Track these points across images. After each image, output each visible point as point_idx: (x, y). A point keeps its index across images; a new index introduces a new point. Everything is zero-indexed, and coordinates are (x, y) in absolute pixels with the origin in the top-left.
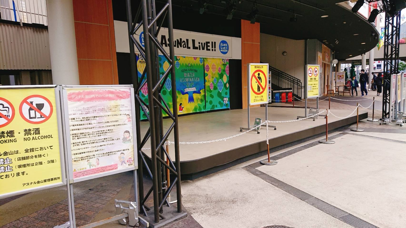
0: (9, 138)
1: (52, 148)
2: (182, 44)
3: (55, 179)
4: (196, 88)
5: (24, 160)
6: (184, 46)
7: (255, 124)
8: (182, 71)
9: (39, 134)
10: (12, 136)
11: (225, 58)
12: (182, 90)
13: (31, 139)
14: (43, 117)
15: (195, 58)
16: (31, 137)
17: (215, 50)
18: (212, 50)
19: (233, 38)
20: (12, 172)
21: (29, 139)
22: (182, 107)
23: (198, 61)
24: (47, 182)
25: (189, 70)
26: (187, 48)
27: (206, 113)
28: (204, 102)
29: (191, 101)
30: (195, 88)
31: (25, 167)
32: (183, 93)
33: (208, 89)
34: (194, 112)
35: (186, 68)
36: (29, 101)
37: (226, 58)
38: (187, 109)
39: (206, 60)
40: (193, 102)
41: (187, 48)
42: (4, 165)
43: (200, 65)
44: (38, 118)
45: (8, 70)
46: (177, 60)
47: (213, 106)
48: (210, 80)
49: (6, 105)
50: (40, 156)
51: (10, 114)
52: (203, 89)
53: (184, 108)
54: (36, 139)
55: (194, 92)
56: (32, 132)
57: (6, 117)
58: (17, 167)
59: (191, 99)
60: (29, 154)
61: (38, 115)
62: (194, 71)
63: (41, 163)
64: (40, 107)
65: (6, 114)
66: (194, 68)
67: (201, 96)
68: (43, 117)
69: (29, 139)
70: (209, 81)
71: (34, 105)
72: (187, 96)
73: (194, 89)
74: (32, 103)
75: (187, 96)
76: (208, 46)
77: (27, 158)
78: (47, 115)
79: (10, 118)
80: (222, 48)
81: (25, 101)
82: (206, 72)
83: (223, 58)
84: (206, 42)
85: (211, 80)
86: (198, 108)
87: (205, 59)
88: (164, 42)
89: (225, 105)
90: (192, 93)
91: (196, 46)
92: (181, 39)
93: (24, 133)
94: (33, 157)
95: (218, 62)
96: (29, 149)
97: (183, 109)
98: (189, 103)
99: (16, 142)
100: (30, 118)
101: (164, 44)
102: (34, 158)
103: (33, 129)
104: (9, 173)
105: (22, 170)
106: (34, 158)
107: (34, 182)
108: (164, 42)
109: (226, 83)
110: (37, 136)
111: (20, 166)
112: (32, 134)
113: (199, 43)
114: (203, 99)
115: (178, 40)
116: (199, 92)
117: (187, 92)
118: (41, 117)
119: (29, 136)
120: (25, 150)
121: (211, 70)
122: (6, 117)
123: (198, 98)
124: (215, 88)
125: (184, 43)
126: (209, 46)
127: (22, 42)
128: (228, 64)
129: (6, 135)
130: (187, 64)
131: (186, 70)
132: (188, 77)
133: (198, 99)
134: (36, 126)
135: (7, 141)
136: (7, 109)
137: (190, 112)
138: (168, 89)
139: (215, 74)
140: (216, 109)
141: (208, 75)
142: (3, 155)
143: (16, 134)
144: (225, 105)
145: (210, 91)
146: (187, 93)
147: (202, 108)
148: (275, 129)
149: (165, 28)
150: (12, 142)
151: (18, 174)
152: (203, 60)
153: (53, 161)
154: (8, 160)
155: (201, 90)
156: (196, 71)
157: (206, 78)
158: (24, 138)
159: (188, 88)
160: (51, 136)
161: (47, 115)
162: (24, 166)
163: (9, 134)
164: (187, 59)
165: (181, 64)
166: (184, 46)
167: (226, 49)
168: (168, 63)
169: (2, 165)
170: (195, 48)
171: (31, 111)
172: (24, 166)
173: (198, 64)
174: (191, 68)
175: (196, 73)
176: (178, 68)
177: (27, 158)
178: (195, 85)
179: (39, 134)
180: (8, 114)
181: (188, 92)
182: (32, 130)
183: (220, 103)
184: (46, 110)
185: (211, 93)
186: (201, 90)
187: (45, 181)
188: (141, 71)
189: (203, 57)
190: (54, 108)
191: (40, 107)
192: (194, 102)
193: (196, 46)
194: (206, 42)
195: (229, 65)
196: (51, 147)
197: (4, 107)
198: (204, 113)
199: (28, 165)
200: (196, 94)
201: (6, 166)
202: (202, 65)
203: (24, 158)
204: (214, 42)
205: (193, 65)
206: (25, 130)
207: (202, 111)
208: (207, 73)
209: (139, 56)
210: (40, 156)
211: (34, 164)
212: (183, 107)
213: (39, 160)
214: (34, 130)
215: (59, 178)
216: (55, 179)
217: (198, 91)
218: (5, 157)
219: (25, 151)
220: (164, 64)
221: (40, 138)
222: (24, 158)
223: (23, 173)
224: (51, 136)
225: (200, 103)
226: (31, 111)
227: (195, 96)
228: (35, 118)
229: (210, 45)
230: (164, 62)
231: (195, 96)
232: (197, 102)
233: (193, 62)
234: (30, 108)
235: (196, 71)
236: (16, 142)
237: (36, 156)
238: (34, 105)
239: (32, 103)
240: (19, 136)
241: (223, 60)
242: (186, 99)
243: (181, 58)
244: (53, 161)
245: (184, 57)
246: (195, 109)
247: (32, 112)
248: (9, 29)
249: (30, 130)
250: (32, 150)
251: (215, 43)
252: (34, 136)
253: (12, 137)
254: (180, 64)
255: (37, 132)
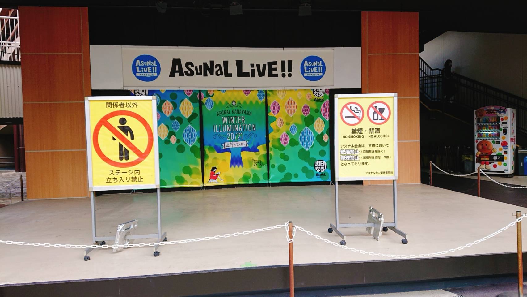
0: (359, 134)
1: (388, 145)
2: (215, 70)
3: (389, 172)
4: (247, 142)
5: (368, 153)
6: (219, 73)
7: (368, 222)
8: (218, 114)
9: (380, 133)
10: (361, 133)
11: (318, 88)
12: (218, 145)
13: (374, 136)
14: (383, 119)
15: (247, 92)
16: (374, 134)
17: (290, 75)
18: (284, 76)
19: (337, 49)
20: (359, 161)
21: (372, 136)
22: (216, 173)
23: (254, 96)
24: (383, 174)
25: (233, 111)
26: (225, 76)
27: (270, 187)
28: (265, 169)
29: (236, 164)
30: (245, 141)
31: (368, 158)
32: (220, 151)
33: (277, 144)
34: (243, 183)
35: (226, 109)
36: (374, 106)
37: (322, 88)
38: (227, 178)
39: (273, 94)
40: (240, 166)
41: (225, 76)
42: (355, 155)
43: (257, 102)
44: (380, 120)
45: (17, 118)
46: (208, 95)
47: (289, 175)
48: (281, 128)
49: (359, 108)
50: (379, 151)
51: (361, 116)
52: (264, 144)
53: (219, 175)
54: (377, 137)
55: (244, 149)
56: (375, 131)
57: (358, 118)
58: (363, 158)
59: (236, 161)
60: (372, 149)
61: (380, 118)
62: (245, 113)
63: (379, 157)
64: (382, 110)
65: (359, 116)
66: (246, 109)
67: (258, 156)
68: (383, 119)
69: (372, 136)
70: (278, 130)
71: (378, 109)
72: (228, 156)
73: (244, 144)
74: (376, 107)
75: (228, 156)
76: (271, 70)
77: (370, 151)
78: (386, 118)
79: (360, 118)
80: (308, 70)
81: (371, 106)
82: (271, 114)
83: (315, 88)
84: (268, 62)
85: (284, 129)
86: (252, 176)
87: (268, 92)
88: (177, 69)
89: (317, 174)
90: (240, 150)
91: (244, 70)
92: (212, 62)
93: (352, 132)
94: (374, 151)
95: (303, 95)
96: (371, 144)
97: (218, 177)
98: (231, 166)
99: (363, 137)
100: (374, 119)
101: (177, 72)
102: (375, 152)
103: (376, 129)
104: (357, 162)
105: (365, 161)
106: (375, 152)
107: (374, 172)
108: (177, 69)
109: (322, 134)
110: (378, 134)
111: (364, 158)
112: (374, 133)
113: (252, 65)
114: (264, 161)
115: (205, 64)
116: (255, 150)
117: (229, 149)
118: (382, 120)
119: (372, 134)
120: (369, 145)
121: (283, 110)
122: (358, 118)
123: (253, 160)
124: (293, 143)
125: (218, 68)
126: (275, 69)
127: (9, 85)
128: (329, 98)
129: (357, 131)
130: (230, 103)
131: (226, 112)
132: (230, 124)
133: (251, 161)
134: (378, 127)
135: (358, 136)
136: (359, 112)
137: (234, 182)
138: (188, 144)
139: (293, 117)
140: (293, 180)
141: (277, 120)
142: (354, 147)
143: (364, 131)
144: (317, 174)
145: (282, 148)
146: (228, 150)
147: (261, 177)
148: (404, 242)
149: (179, 47)
150: (361, 137)
151: (363, 164)
152: (266, 94)
153: (388, 157)
154: (357, 151)
155: (259, 145)
156: (248, 113)
157: (272, 125)
158: (369, 136)
159: (229, 143)
160: (388, 136)
161: (386, 118)
162: (368, 157)
163: (359, 131)
164: (229, 94)
165: (217, 103)
166: (219, 73)
167: (318, 71)
168: (190, 102)
169: (353, 155)
170: (241, 73)
171: (375, 114)
172: (368, 157)
173: (254, 102)
174: (238, 108)
175: (247, 116)
176: (210, 110)
177: (370, 151)
178: (247, 137)
179: (380, 133)
180: (360, 116)
181: (231, 150)
182: (374, 129)
183: (304, 170)
184: (385, 114)
185: (282, 152)
186: (259, 146)
187: (381, 173)
188: (185, 114)
189: (265, 89)
190: (392, 112)
191: (382, 110)
192: (242, 166)
193: (244, 70)
194: (268, 62)
195: (330, 100)
196: (387, 144)
197: (357, 110)
198: (266, 186)
199: (370, 157)
200: (247, 152)
201: (356, 155)
202: (262, 103)
203: (368, 152)
204: (288, 61)
205: (242, 103)
206: (370, 129)
207: (260, 182)
208: (275, 116)
209: (316, 167)
210: (379, 151)
211: (375, 158)
212: (217, 174)
213: (378, 154)
214: (376, 129)
215: (392, 172)
216: (389, 172)
217: (253, 147)
218: (356, 149)
219: (368, 146)
220: (182, 104)
221: (380, 136)
222: (368, 152)
223: (366, 163)
224: (388, 136)
225: (256, 168)
226: (375, 114)
227: (245, 156)
228: (377, 119)
229: (279, 66)
230: (182, 100)
231: (245, 156)
232: (251, 166)
233: (241, 97)
234: (375, 111)
235: (248, 113)
236: (363, 137)
237: (376, 151)
238: (378, 109)
239: (376, 107)
240: (366, 134)
241: (314, 92)
242: (224, 160)
243: (217, 94)
244: (388, 157)
245: (224, 91)
246: (246, 177)
247: (376, 115)
248: (17, 71)
249: (373, 129)
250: (374, 145)
251: (290, 63)
252: (376, 134)
253: (361, 133)
254: (214, 102)
255: (378, 131)
